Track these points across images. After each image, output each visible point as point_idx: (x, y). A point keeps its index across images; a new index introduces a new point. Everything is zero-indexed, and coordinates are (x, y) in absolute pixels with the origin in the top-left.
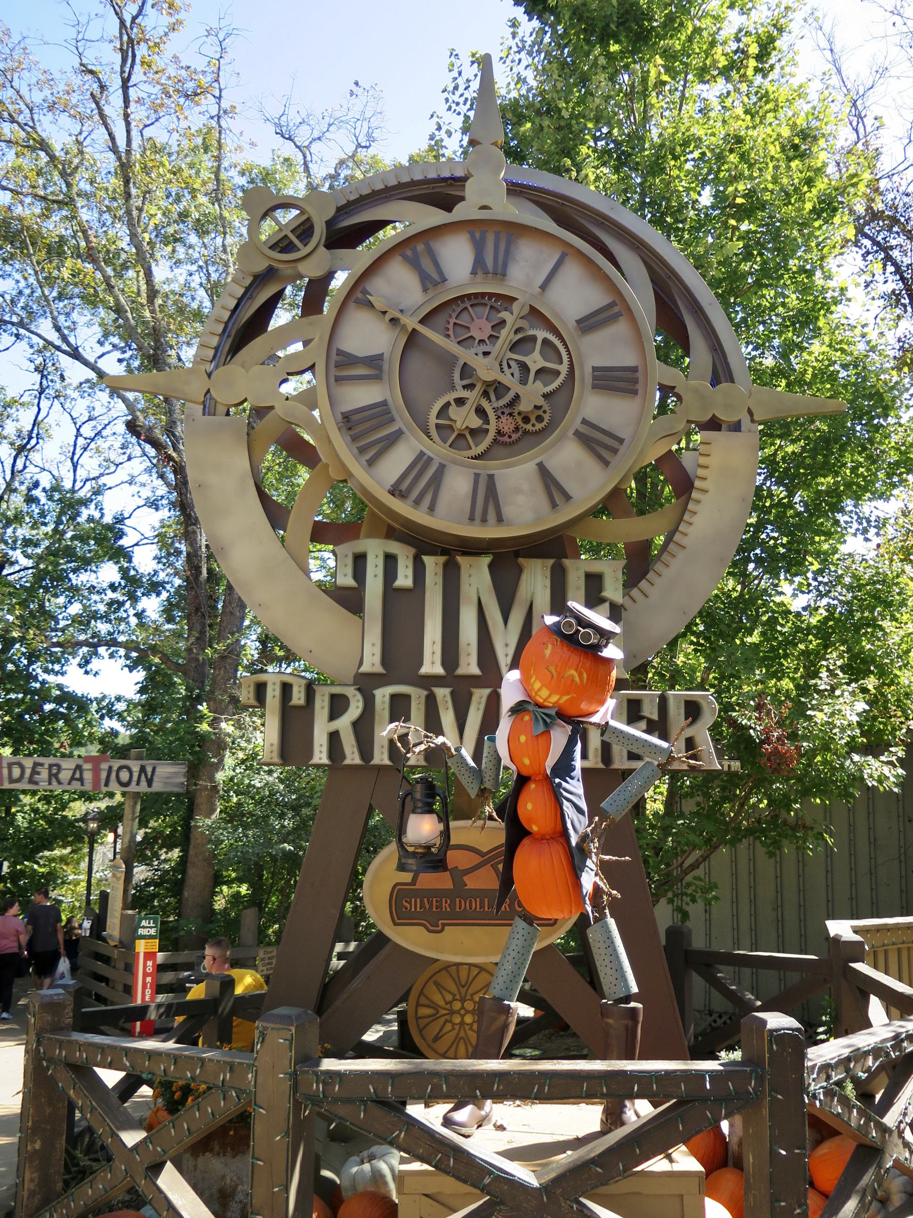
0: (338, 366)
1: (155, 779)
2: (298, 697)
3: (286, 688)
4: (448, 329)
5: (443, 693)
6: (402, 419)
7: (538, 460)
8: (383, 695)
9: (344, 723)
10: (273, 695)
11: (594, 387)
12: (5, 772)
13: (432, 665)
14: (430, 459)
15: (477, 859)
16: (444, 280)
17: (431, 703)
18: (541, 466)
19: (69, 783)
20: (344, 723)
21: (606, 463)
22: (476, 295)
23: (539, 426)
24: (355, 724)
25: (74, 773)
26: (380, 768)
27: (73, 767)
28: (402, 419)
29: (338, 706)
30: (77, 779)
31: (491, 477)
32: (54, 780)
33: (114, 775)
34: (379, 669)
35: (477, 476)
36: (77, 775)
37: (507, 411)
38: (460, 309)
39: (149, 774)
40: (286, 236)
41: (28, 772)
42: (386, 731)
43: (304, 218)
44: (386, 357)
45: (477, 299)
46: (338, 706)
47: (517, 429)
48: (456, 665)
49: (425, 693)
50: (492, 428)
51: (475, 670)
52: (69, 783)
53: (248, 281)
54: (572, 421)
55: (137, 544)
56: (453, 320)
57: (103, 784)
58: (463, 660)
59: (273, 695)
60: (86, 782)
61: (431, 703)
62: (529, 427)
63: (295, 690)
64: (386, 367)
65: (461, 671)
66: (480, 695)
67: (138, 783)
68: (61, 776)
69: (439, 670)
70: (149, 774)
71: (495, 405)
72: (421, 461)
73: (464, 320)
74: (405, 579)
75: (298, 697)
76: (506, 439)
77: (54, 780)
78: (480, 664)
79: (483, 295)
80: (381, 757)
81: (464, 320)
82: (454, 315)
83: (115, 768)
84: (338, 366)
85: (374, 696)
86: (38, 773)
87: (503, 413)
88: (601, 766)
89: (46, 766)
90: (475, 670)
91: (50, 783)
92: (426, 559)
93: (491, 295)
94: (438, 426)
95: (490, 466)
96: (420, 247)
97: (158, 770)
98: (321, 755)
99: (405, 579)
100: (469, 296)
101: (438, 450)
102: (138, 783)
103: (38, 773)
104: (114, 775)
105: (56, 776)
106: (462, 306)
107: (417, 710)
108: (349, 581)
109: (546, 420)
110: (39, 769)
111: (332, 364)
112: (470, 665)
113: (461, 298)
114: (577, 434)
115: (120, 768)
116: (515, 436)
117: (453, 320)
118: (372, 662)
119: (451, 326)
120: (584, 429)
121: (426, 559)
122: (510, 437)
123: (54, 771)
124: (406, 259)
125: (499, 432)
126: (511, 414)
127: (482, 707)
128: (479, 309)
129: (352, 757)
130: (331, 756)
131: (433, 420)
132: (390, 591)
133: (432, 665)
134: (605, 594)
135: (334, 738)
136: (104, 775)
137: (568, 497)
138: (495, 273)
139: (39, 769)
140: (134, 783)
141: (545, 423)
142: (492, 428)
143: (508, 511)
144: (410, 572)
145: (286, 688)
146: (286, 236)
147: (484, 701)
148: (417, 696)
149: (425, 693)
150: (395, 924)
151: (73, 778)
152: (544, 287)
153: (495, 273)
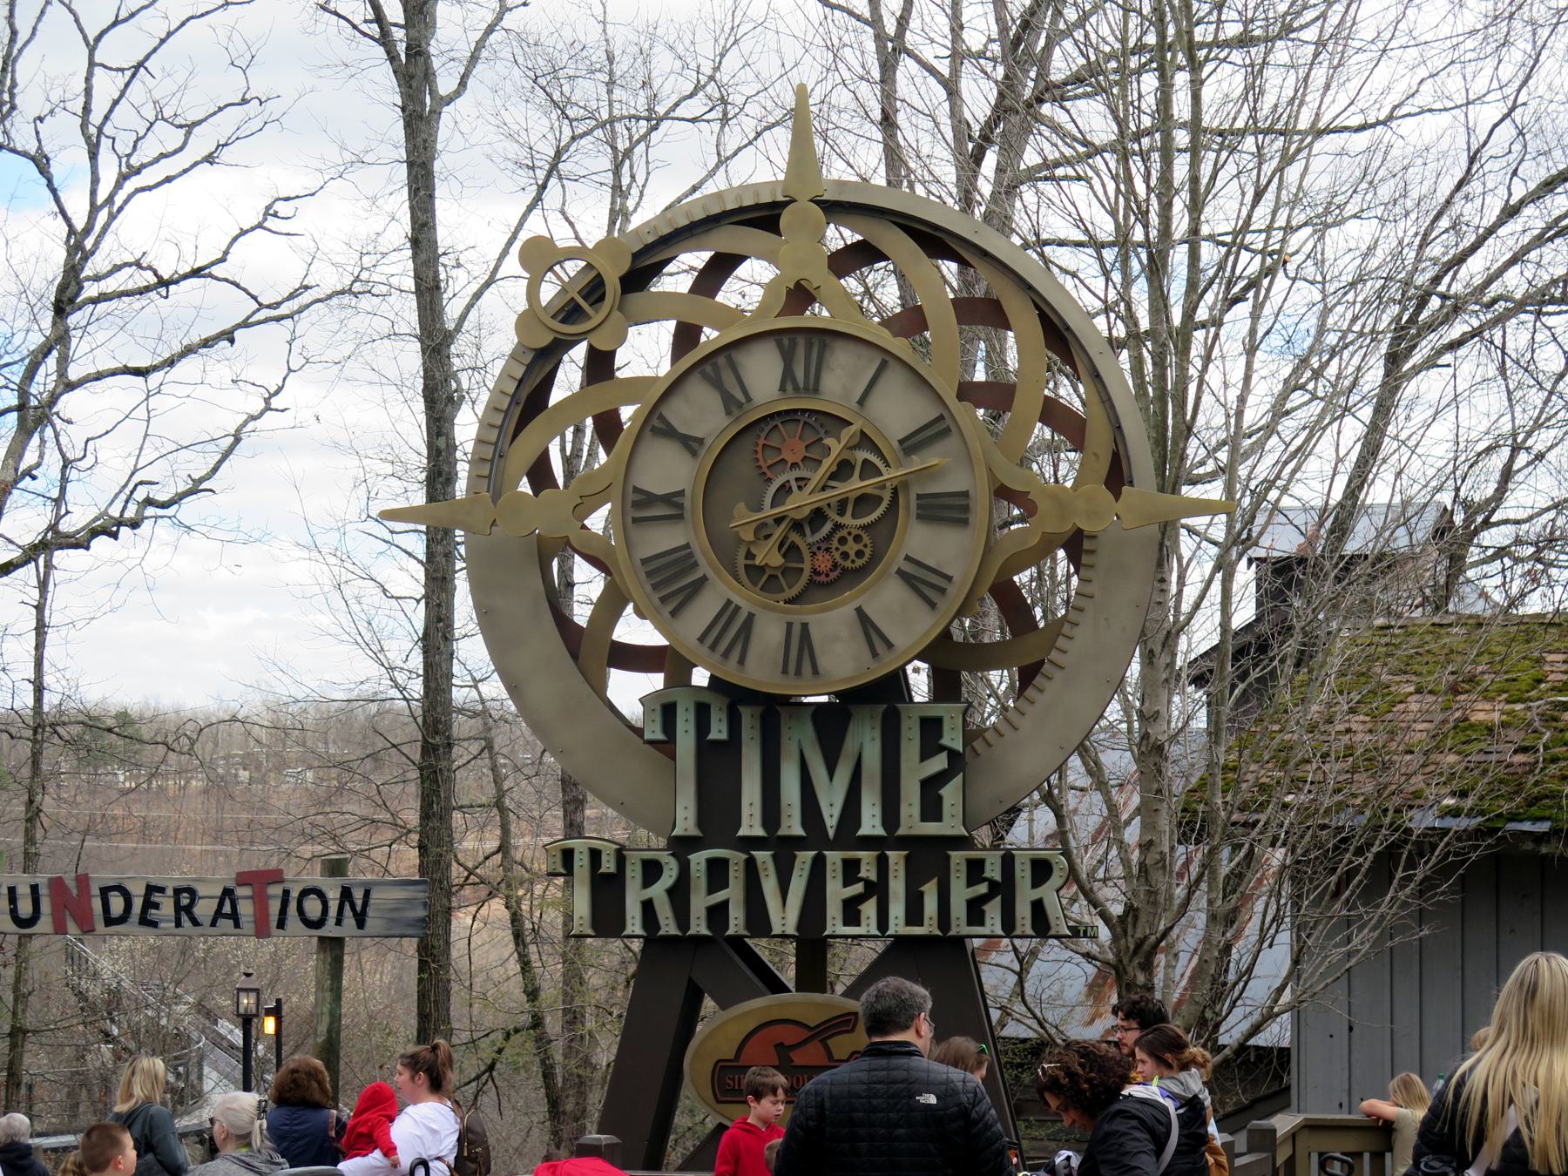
0: (637, 505)
1: (370, 912)
2: (608, 865)
3: (595, 855)
4: (756, 452)
5: (763, 857)
6: (706, 563)
7: (856, 604)
8: (698, 860)
9: (658, 891)
10: (581, 862)
11: (919, 517)
12: (97, 904)
13: (752, 825)
14: (738, 608)
15: (806, 1034)
16: (749, 399)
17: (751, 867)
18: (859, 611)
19: (213, 924)
20: (658, 891)
21: (932, 605)
22: (787, 412)
23: (860, 562)
24: (670, 892)
25: (221, 905)
26: (699, 939)
27: (219, 892)
28: (706, 563)
29: (652, 871)
30: (226, 916)
31: (805, 626)
32: (185, 918)
33: (293, 906)
34: (693, 831)
35: (790, 625)
36: (227, 909)
37: (824, 546)
38: (770, 427)
39: (359, 903)
40: (572, 299)
41: (138, 904)
42: (700, 902)
43: (593, 274)
44: (688, 493)
45: (789, 416)
46: (652, 871)
47: (835, 565)
48: (778, 825)
49: (745, 856)
50: (807, 567)
51: (798, 831)
52: (213, 924)
53: (528, 359)
54: (895, 558)
55: (245, 324)
56: (762, 442)
57: (274, 923)
58: (784, 822)
59: (581, 862)
60: (243, 920)
61: (751, 867)
62: (848, 564)
63: (604, 858)
64: (687, 504)
65: (782, 832)
66: (805, 857)
67: (339, 922)
68: (197, 911)
69: (759, 831)
70: (359, 903)
71: (810, 539)
72: (729, 611)
73: (774, 441)
74: (718, 731)
75: (608, 865)
76: (823, 579)
77: (185, 918)
78: (804, 825)
79: (795, 411)
80: (699, 927)
81: (774, 441)
82: (763, 435)
83: (295, 894)
84: (637, 505)
85: (689, 861)
86: (156, 906)
87: (819, 548)
88: (938, 933)
89: (170, 892)
90: (798, 831)
91: (178, 924)
92: (741, 709)
93: (804, 411)
94: (746, 566)
95: (800, 614)
96: (721, 360)
97: (373, 895)
98: (634, 925)
99: (718, 731)
100: (779, 413)
101: (745, 599)
102: (339, 922)
103: (156, 906)
104: (293, 906)
105: (188, 910)
106: (772, 424)
107: (736, 875)
108: (660, 736)
109: (867, 556)
110: (156, 897)
111: (629, 504)
112: (793, 825)
113: (772, 416)
114: (900, 572)
115: (305, 893)
116: (833, 575)
117: (762, 442)
118: (686, 822)
119: (759, 449)
120: (909, 568)
121: (741, 709)
122: (827, 575)
123: (185, 902)
124: (705, 377)
125: (815, 572)
126: (827, 550)
127: (806, 873)
128: (791, 426)
129: (668, 927)
130: (645, 925)
131: (741, 561)
132: (705, 747)
133: (752, 825)
134: (945, 741)
135: (648, 907)
136: (275, 907)
137: (889, 645)
138: (806, 389)
139: (156, 897)
140: (331, 921)
141: (865, 559)
142: (807, 567)
143: (823, 662)
144: (724, 727)
145: (595, 855)
146: (572, 299)
147: (807, 867)
148: (736, 858)
149: (745, 856)
150: (718, 1102)
151: (219, 914)
152: (861, 402)
153: (806, 389)
